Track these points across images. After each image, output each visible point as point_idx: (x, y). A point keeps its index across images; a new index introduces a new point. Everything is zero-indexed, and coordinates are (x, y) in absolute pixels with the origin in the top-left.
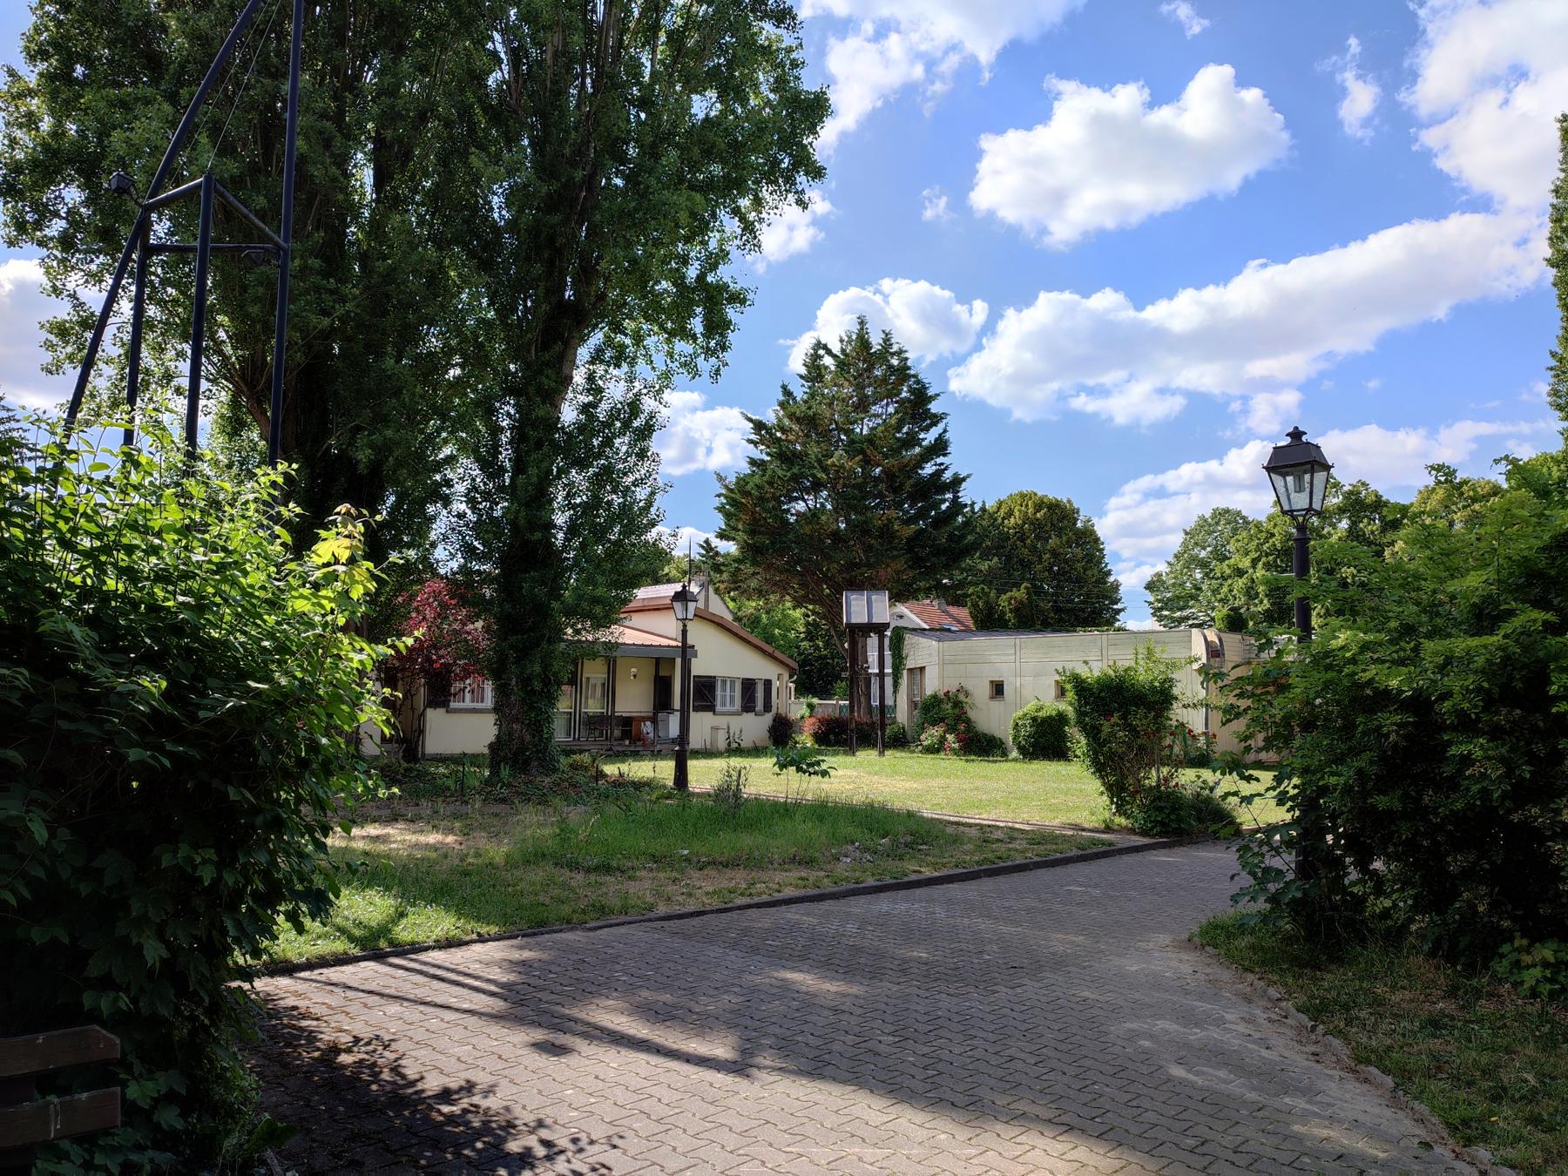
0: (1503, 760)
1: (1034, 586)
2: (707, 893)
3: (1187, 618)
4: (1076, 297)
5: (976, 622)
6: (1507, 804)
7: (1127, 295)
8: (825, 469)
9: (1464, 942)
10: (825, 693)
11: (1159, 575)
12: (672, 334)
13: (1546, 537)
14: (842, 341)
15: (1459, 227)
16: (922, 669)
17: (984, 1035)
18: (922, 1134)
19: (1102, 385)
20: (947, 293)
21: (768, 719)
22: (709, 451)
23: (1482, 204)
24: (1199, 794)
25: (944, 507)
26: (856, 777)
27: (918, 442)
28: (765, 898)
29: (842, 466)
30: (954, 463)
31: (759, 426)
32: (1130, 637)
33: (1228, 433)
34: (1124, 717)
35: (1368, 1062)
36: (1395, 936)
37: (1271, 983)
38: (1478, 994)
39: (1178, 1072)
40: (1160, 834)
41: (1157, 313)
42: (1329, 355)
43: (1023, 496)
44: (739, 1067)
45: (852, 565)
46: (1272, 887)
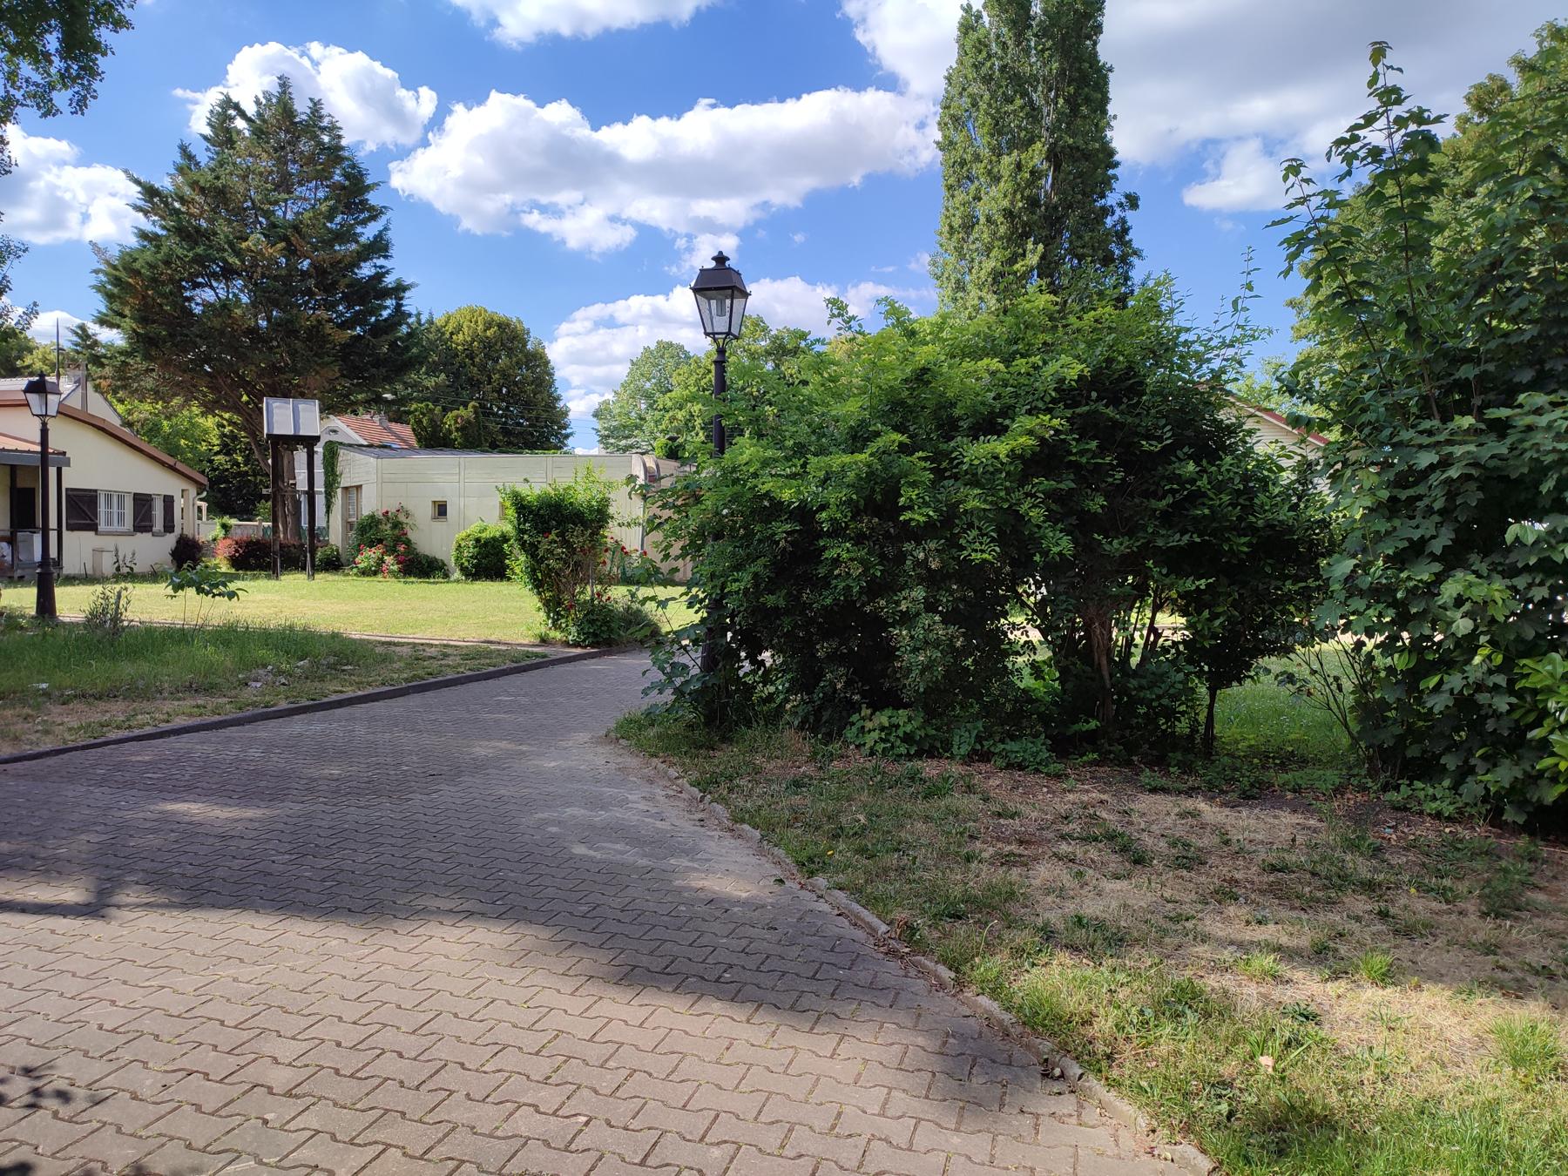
0: (862, 562)
1: (482, 406)
2: (70, 729)
3: (631, 447)
4: (530, 104)
5: (419, 441)
6: (865, 598)
7: (583, 112)
8: (238, 253)
9: (826, 716)
10: (246, 513)
11: (606, 402)
12: (15, 51)
13: (908, 370)
14: (258, 102)
15: (872, 99)
16: (359, 487)
17: (393, 841)
18: (311, 944)
19: (556, 205)
20: (389, 73)
21: (170, 540)
22: (86, 218)
23: (891, 83)
24: (629, 608)
25: (385, 313)
26: (270, 601)
27: (354, 238)
28: (148, 730)
29: (260, 252)
30: (398, 268)
31: (150, 192)
32: (583, 465)
33: (674, 269)
34: (561, 534)
35: (743, 821)
36: (774, 718)
37: (672, 765)
38: (831, 757)
39: (580, 850)
40: (592, 645)
41: (614, 137)
42: (765, 205)
43: (473, 311)
44: (93, 910)
45: (275, 369)
46: (678, 681)
